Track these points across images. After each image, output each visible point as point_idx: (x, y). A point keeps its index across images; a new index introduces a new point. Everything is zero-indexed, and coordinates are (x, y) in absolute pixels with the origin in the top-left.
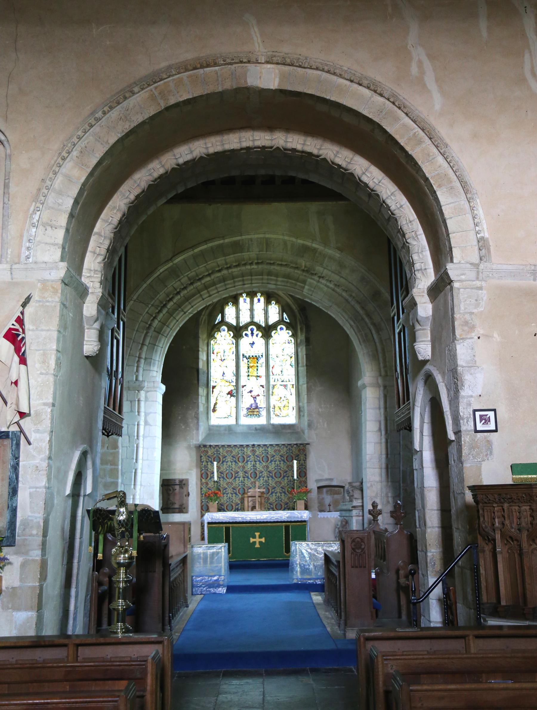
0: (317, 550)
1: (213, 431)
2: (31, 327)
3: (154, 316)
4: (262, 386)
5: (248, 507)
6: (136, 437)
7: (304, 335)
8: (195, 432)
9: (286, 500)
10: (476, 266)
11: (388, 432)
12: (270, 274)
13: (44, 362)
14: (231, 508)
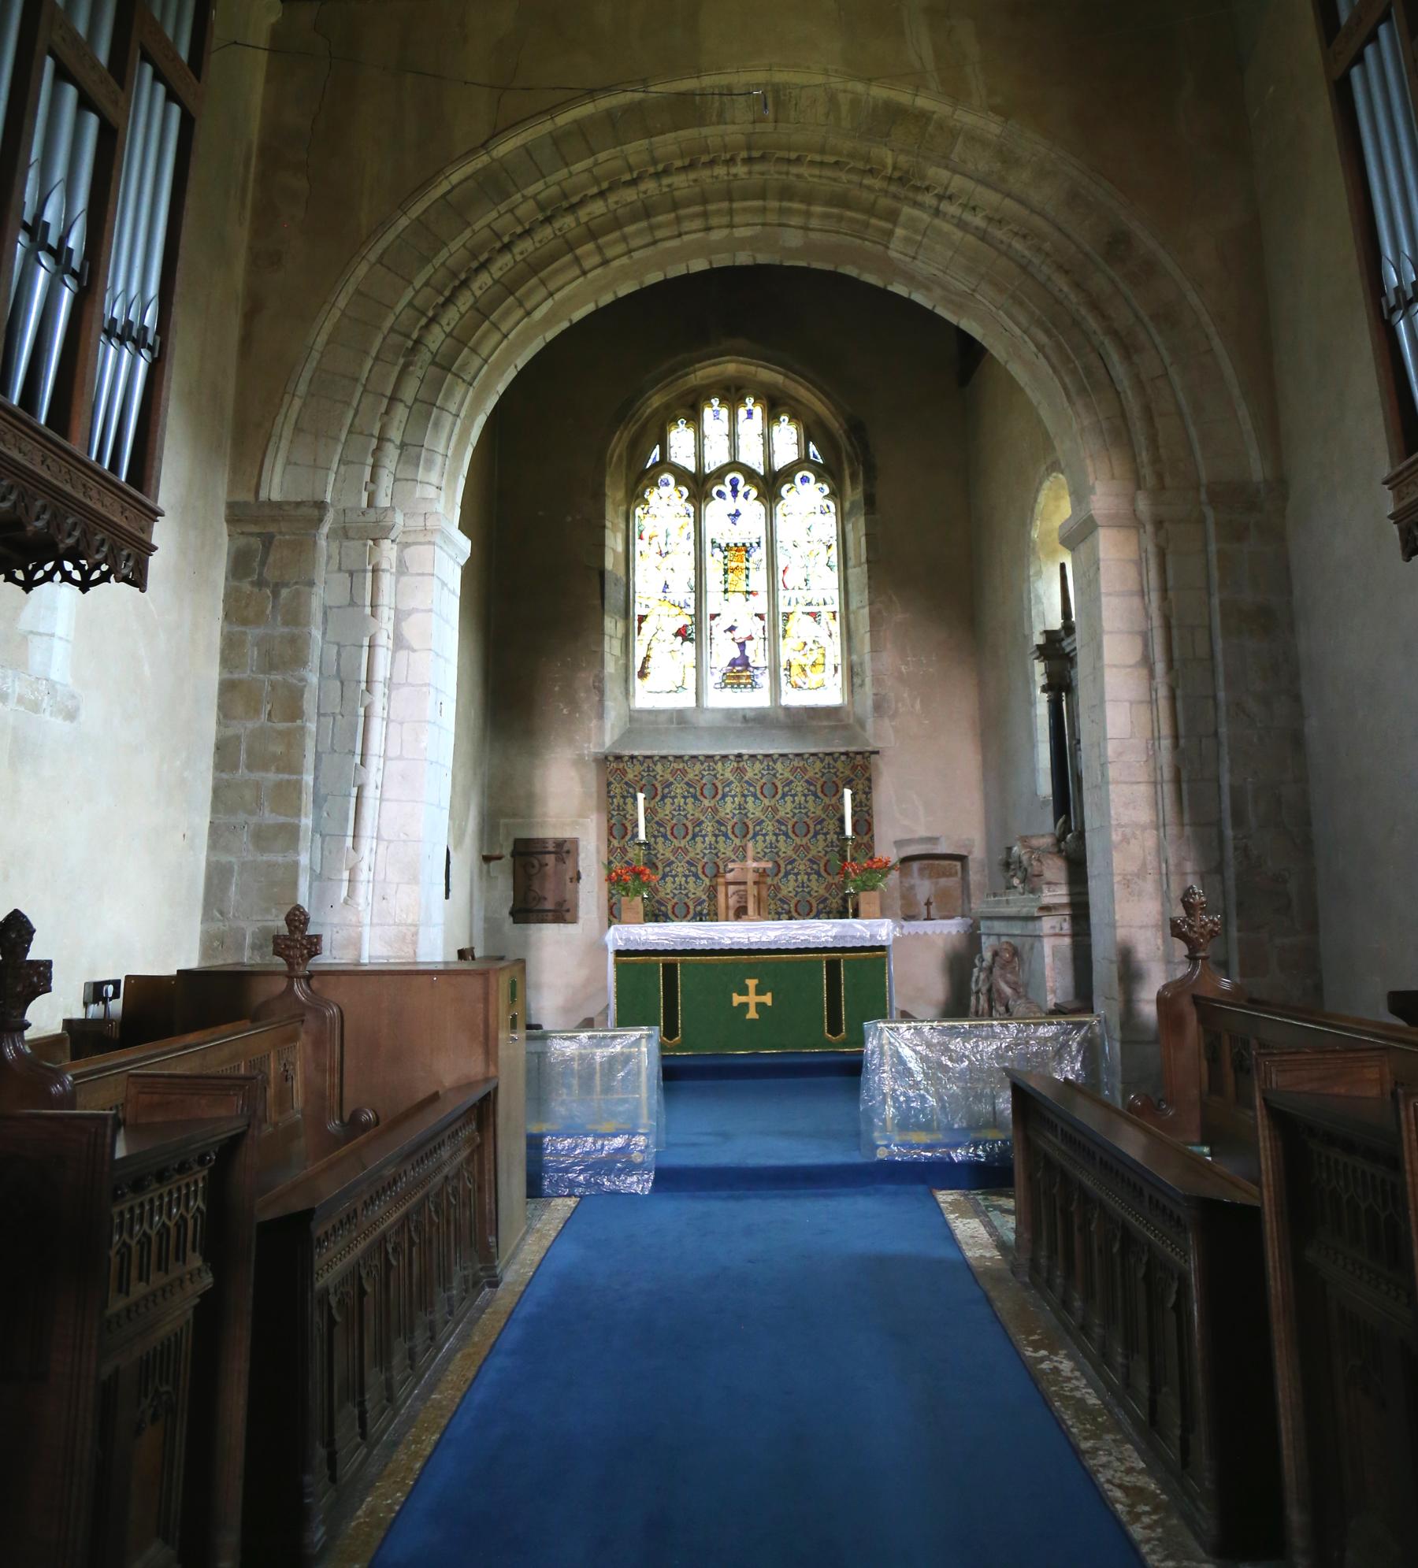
0: (948, 1049)
1: (640, 722)
3: (430, 314)
4: (761, 616)
5: (727, 908)
6: (363, 686)
7: (860, 490)
8: (594, 723)
9: (822, 892)
11: (1177, 665)
12: (786, 193)
14: (807, 909)
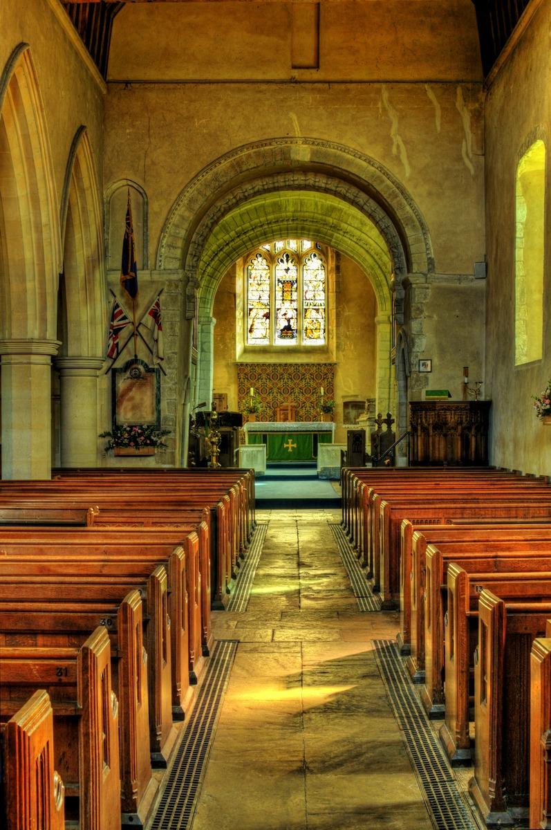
2: (163, 308)
7: (334, 263)
10: (425, 275)
13: (172, 328)
